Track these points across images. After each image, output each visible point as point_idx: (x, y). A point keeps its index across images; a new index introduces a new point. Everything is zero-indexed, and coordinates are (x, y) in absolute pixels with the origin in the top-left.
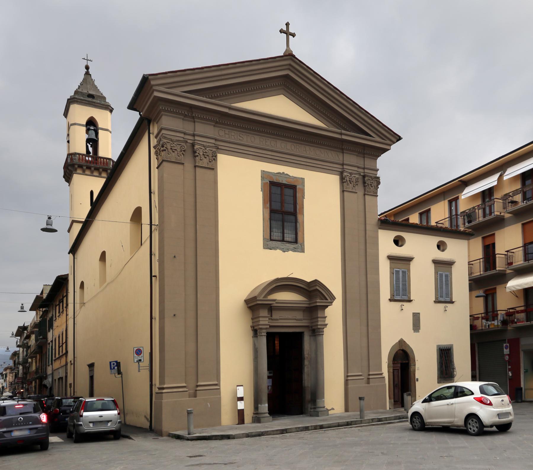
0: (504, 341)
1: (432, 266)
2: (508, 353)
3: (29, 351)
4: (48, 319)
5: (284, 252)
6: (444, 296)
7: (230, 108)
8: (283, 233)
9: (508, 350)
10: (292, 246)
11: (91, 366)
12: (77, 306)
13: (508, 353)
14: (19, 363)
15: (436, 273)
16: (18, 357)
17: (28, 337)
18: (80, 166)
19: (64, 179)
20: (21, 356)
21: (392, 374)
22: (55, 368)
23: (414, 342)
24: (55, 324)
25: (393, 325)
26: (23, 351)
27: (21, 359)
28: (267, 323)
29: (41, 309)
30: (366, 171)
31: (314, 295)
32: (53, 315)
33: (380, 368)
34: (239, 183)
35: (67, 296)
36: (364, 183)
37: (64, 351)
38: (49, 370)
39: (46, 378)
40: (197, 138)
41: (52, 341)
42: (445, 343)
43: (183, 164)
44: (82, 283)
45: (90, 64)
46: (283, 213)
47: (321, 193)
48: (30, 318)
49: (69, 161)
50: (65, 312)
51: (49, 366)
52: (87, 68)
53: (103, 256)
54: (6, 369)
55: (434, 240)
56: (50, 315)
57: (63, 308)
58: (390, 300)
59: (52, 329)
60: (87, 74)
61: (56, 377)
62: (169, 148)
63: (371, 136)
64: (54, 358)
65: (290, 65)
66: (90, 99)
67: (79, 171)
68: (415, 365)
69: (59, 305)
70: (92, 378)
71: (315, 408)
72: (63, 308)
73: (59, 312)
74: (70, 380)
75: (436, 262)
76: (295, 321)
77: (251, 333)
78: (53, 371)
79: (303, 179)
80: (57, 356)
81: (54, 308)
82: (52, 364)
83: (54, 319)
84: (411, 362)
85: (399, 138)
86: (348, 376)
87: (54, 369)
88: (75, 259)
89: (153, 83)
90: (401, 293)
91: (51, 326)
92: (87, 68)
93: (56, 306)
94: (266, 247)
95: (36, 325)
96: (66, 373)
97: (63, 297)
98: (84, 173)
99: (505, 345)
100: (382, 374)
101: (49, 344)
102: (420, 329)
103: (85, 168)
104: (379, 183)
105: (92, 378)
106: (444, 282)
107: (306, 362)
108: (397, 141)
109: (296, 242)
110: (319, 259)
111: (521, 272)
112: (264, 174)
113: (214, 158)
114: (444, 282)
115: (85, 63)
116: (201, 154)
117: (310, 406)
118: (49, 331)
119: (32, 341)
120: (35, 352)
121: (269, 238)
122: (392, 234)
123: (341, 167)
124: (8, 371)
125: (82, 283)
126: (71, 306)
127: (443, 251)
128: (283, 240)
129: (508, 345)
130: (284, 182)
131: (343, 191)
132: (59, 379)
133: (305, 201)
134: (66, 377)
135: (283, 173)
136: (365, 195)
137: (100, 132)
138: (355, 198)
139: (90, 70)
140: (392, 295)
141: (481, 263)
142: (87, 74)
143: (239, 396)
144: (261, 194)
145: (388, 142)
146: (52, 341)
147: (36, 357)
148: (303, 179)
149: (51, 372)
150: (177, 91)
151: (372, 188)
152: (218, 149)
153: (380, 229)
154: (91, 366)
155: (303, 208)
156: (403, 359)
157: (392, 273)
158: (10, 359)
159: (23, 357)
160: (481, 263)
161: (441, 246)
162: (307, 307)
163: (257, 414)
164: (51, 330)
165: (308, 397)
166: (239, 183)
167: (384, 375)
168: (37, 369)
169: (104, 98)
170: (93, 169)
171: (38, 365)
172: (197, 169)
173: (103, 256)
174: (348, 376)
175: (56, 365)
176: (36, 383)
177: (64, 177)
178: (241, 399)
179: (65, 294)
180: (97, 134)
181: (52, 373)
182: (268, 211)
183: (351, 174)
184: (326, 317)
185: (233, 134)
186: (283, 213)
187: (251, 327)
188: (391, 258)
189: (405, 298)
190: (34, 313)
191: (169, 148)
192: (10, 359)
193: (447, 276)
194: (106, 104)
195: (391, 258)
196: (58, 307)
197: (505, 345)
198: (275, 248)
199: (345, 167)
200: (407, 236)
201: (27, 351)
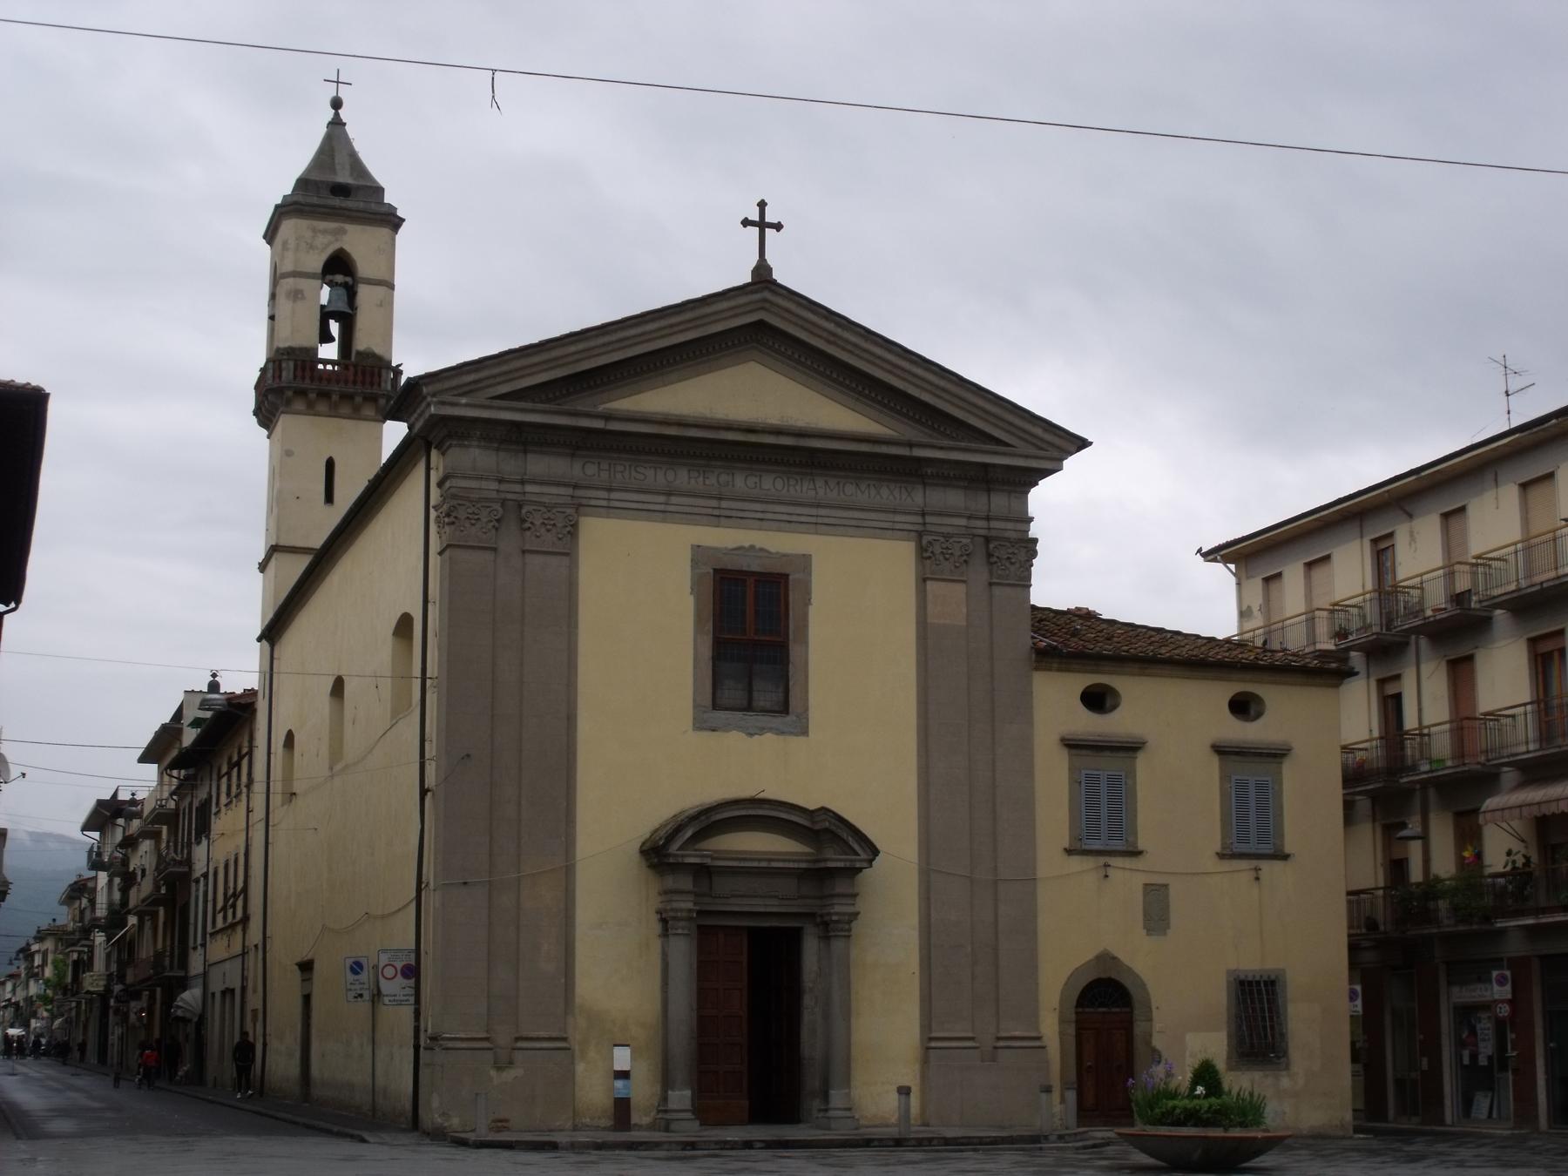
0: (1497, 962)
1: (1215, 760)
2: (1509, 996)
3: (133, 892)
4: (196, 804)
5: (751, 735)
6: (1252, 837)
7: (608, 417)
8: (750, 692)
9: (1508, 987)
10: (777, 721)
11: (306, 967)
12: (276, 800)
13: (1509, 996)
14: (95, 924)
15: (1224, 777)
16: (92, 902)
17: (129, 843)
18: (301, 393)
19: (255, 419)
20: (102, 899)
21: (1072, 1041)
22: (212, 958)
23: (1143, 958)
24: (218, 825)
25: (1078, 919)
26: (110, 882)
27: (101, 911)
28: (690, 905)
29: (175, 773)
30: (994, 524)
31: (832, 849)
32: (210, 795)
33: (1033, 1017)
34: (637, 580)
35: (250, 753)
36: (989, 555)
37: (239, 914)
38: (196, 964)
39: (183, 984)
40: (529, 488)
41: (205, 876)
42: (1252, 963)
43: (495, 550)
44: (290, 737)
45: (344, 93)
46: (751, 642)
47: (861, 594)
48: (143, 782)
49: (270, 374)
50: (244, 797)
51: (195, 948)
52: (337, 104)
53: (338, 687)
54: (40, 936)
55: (1220, 692)
56: (202, 794)
57: (239, 786)
58: (1069, 852)
59: (208, 837)
60: (337, 124)
61: (216, 986)
62: (938, 550)
63: (1007, 445)
64: (209, 929)
65: (765, 300)
66: (337, 201)
67: (299, 405)
68: (1150, 1020)
69: (229, 774)
70: (307, 999)
71: (826, 1110)
72: (239, 786)
73: (228, 794)
74: (254, 1001)
75: (1221, 750)
76: (776, 902)
77: (657, 928)
78: (208, 966)
79: (806, 559)
80: (220, 924)
81: (215, 777)
82: (204, 945)
83: (214, 809)
84: (1138, 1012)
85: (1082, 444)
86: (931, 1039)
87: (214, 957)
88: (276, 663)
89: (425, 390)
90: (1105, 831)
91: (204, 829)
92: (337, 104)
93: (220, 778)
94: (700, 725)
95: (162, 816)
96: (244, 978)
97: (241, 758)
98: (311, 410)
99: (1495, 974)
100: (1039, 1038)
101: (197, 881)
102: (1168, 926)
103: (312, 396)
104: (1034, 554)
105: (307, 999)
106: (1253, 804)
107: (807, 1000)
108: (1079, 449)
109: (784, 709)
110: (855, 745)
111: (1535, 771)
112: (697, 550)
113: (573, 531)
114: (1253, 804)
115: (331, 91)
116: (538, 523)
117: (817, 1104)
118: (199, 843)
119: (144, 857)
120: (154, 901)
121: (708, 702)
122: (1079, 682)
123: (919, 519)
124: (49, 944)
125: (290, 737)
126: (259, 787)
127: (1259, 715)
128: (749, 707)
129: (1508, 973)
130: (755, 568)
131: (923, 580)
132: (224, 993)
133: (813, 611)
134: (244, 989)
135: (752, 547)
136: (991, 584)
137: (364, 292)
138: (951, 600)
139: (344, 114)
140: (1076, 837)
141: (1529, 716)
142: (337, 124)
143: (617, 1067)
144: (690, 602)
145: (1056, 454)
146: (205, 876)
147: (154, 916)
148: (806, 559)
149: (201, 970)
150: (481, 397)
151: (1012, 568)
152: (580, 507)
153: (1036, 669)
154: (306, 967)
155: (806, 626)
156: (1106, 1001)
157: (1074, 782)
158: (62, 903)
159: (110, 904)
160: (1529, 716)
161: (1242, 707)
162: (806, 870)
163: (666, 1111)
164: (204, 842)
165: (812, 1082)
166: (637, 580)
167: (1046, 1041)
168: (158, 956)
169: (380, 191)
170: (335, 397)
171: (160, 945)
172: (529, 557)
173: (338, 687)
174: (931, 1039)
175: (218, 949)
176: (152, 997)
177: (256, 413)
178: (624, 1075)
179: (245, 750)
180: (352, 294)
181: (205, 974)
182: (707, 641)
183: (947, 536)
184: (855, 896)
185: (619, 468)
186: (751, 642)
187: (659, 912)
188: (1073, 745)
189: (1118, 845)
190: (152, 770)
191: (938, 550)
192: (62, 903)
193: (1262, 788)
194: (383, 209)
195: (1073, 745)
196: (224, 780)
197: (1495, 974)
198: (726, 728)
199: (929, 519)
200: (1125, 684)
201: (125, 891)
